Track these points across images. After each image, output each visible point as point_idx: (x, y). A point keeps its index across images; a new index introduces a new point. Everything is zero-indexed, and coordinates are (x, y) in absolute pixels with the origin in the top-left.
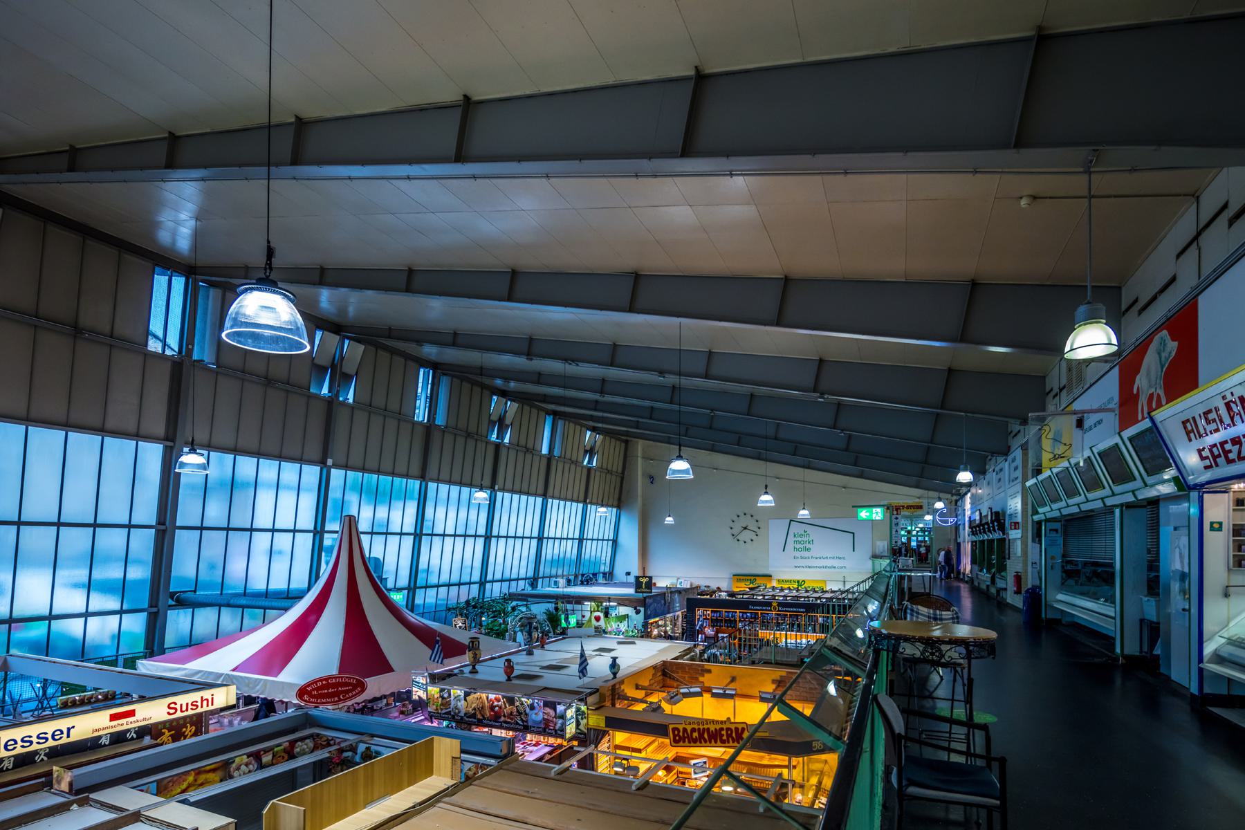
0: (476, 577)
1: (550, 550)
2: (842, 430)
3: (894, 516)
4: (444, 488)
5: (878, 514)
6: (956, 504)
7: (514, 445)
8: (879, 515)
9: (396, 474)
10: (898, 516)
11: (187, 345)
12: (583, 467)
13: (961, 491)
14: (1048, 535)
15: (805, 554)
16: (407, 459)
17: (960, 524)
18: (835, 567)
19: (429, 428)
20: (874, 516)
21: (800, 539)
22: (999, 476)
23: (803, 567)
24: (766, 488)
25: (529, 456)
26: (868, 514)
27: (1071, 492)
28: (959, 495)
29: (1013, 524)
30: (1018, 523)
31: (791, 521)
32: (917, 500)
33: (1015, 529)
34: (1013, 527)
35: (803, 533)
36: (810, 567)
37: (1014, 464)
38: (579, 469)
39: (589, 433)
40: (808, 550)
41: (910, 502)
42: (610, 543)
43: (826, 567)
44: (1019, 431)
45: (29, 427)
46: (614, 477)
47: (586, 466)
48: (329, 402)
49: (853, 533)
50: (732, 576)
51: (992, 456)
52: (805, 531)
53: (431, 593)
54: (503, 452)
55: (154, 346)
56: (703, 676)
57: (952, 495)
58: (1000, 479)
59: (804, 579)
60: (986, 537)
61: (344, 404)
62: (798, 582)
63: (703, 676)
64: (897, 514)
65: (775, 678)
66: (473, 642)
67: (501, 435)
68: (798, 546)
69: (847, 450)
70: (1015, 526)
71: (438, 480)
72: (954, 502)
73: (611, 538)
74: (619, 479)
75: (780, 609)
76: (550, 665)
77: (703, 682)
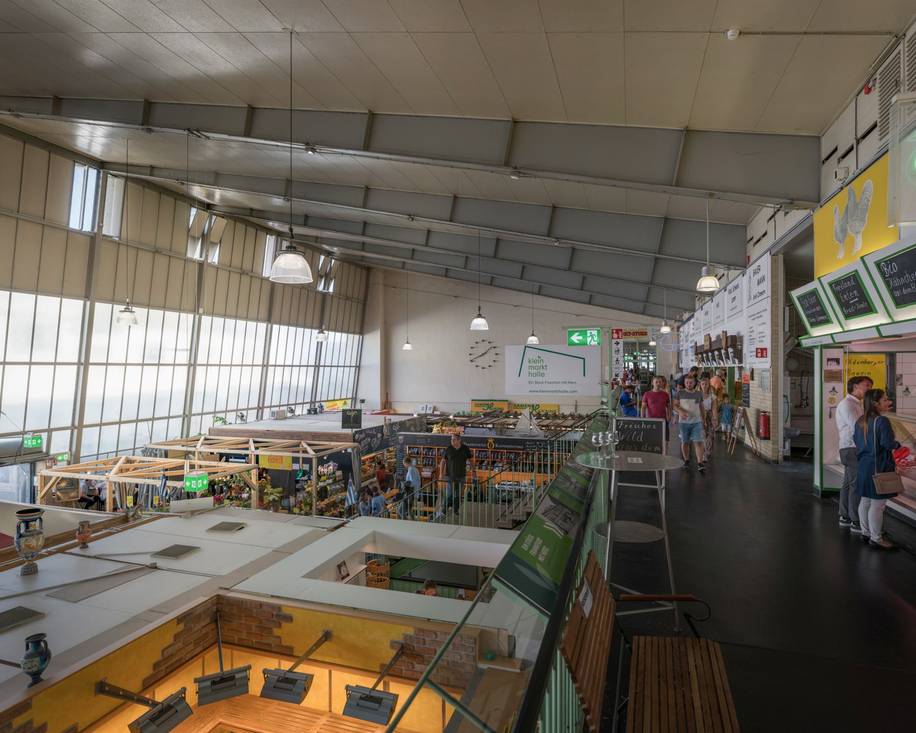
0: (178, 409)
1: (276, 377)
2: (558, 238)
3: (614, 341)
4: (219, 321)
5: (593, 338)
6: (678, 330)
7: (225, 267)
8: (596, 339)
9: (116, 301)
10: (618, 340)
11: (99, 224)
12: (317, 292)
13: (684, 317)
14: (825, 368)
15: (539, 379)
16: (257, 302)
17: (682, 350)
18: (567, 392)
19: (94, 240)
20: (589, 339)
21: (534, 365)
22: (732, 295)
23: (537, 391)
24: (479, 310)
25: (161, 261)
26: (581, 338)
27: (156, 455)
28: (682, 321)
29: (759, 351)
30: (766, 349)
31: (526, 347)
32: (642, 327)
33: (762, 356)
34: (759, 355)
35: (538, 359)
36: (543, 392)
37: (759, 276)
38: (312, 295)
39: (322, 257)
40: (543, 375)
41: (636, 328)
42: (353, 369)
43: (559, 391)
44: (723, 275)
45: (97, 304)
46: (354, 304)
47: (321, 293)
48: (91, 237)
49: (584, 359)
50: (471, 401)
51: (701, 296)
52: (539, 357)
53: (110, 433)
54: (209, 275)
55: (74, 224)
56: (280, 626)
57: (676, 321)
58: (734, 298)
59: (537, 403)
60: (715, 365)
61: (210, 265)
62: (533, 406)
63: (280, 626)
64: (618, 338)
65: (396, 639)
66: (27, 523)
67: (327, 285)
68: (532, 371)
69: (570, 269)
70: (762, 353)
71: (212, 314)
72: (676, 329)
73: (353, 364)
74: (360, 306)
75: (496, 446)
76: (223, 523)
77: (279, 637)
